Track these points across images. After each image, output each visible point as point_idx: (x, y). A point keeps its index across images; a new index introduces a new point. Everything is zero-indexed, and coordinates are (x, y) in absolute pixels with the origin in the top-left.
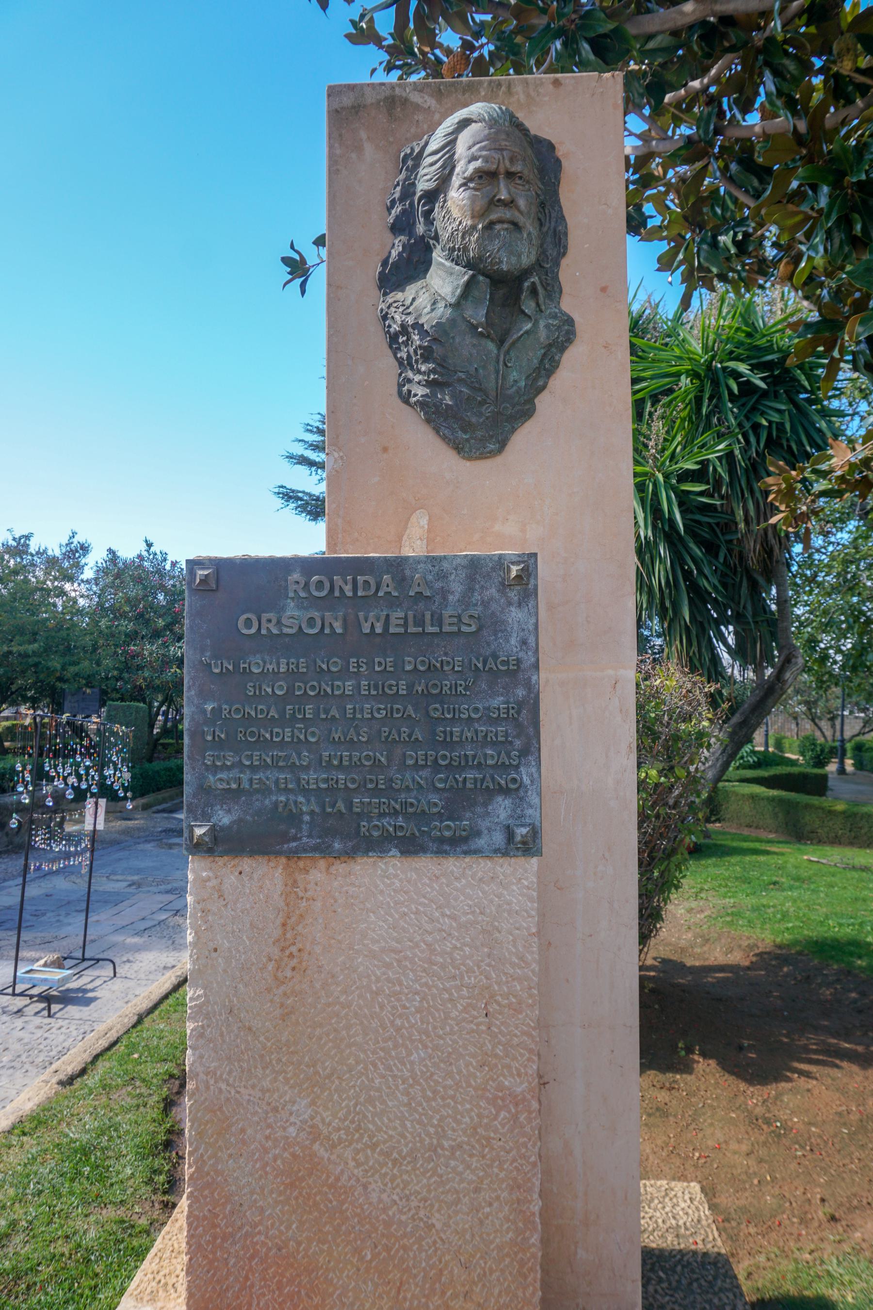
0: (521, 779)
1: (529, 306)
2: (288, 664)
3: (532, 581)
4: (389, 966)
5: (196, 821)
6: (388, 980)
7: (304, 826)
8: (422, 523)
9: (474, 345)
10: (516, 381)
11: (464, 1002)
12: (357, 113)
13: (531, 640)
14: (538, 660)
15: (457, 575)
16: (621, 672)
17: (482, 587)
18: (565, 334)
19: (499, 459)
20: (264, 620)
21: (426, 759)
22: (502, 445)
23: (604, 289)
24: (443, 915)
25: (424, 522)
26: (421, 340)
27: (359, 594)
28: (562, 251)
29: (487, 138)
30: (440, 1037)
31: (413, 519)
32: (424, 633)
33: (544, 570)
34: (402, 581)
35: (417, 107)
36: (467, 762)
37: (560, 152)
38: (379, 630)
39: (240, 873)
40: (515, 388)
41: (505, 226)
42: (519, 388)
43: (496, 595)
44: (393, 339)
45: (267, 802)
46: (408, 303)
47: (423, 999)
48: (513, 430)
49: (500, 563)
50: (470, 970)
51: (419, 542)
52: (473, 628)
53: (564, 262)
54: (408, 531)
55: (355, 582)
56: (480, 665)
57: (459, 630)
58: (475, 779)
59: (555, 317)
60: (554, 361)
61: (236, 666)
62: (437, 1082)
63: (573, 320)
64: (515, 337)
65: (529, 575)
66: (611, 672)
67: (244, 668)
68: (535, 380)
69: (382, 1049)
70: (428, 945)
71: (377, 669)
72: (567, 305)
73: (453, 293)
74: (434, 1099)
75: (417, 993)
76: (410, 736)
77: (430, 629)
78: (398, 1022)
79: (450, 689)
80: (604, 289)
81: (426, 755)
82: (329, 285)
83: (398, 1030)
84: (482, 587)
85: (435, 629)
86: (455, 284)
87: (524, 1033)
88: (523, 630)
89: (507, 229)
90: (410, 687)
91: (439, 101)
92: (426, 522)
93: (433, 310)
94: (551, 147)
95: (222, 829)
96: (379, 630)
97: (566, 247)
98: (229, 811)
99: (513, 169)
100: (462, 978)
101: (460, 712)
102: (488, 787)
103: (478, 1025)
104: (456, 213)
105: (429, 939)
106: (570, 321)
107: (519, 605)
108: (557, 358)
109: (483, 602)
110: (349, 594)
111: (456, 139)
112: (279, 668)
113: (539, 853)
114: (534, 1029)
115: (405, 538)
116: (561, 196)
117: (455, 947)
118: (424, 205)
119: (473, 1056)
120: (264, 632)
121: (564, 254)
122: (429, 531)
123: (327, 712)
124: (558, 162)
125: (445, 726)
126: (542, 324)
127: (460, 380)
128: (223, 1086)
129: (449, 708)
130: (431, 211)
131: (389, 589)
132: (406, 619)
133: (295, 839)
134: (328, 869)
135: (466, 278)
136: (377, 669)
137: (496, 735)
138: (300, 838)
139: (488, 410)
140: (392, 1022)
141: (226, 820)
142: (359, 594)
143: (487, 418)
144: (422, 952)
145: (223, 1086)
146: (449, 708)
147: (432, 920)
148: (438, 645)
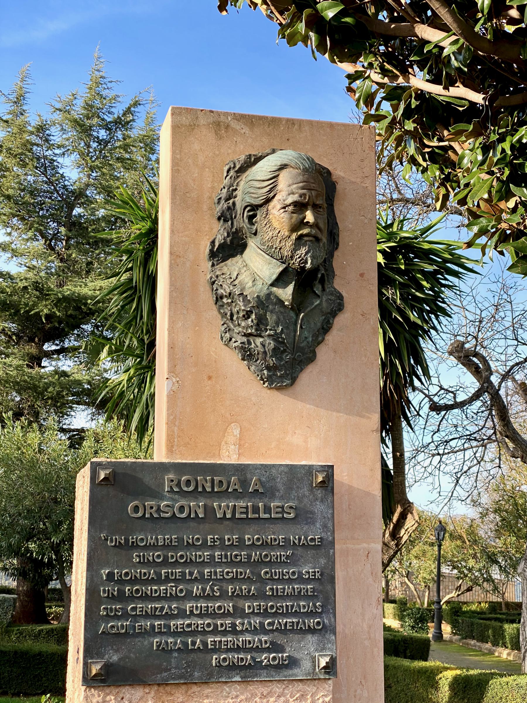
0: (324, 622)
1: (318, 289)
2: (164, 539)
3: (331, 485)
5: (92, 658)
7: (173, 660)
8: (235, 433)
9: (281, 312)
10: (306, 338)
12: (193, 129)
13: (330, 525)
14: (334, 538)
15: (281, 478)
16: (373, 545)
17: (298, 487)
18: (338, 305)
20: (148, 508)
21: (260, 609)
23: (362, 275)
25: (237, 432)
26: (245, 306)
27: (216, 490)
29: (301, 178)
32: (259, 518)
33: (338, 476)
34: (244, 483)
35: (235, 131)
36: (287, 610)
38: (229, 516)
39: (122, 698)
40: (305, 343)
41: (311, 238)
42: (308, 342)
43: (307, 493)
44: (219, 298)
45: (146, 643)
46: (234, 277)
48: (302, 370)
49: (309, 470)
51: (233, 447)
52: (292, 515)
54: (225, 438)
55: (213, 481)
56: (296, 542)
57: (283, 516)
58: (293, 622)
59: (332, 294)
60: (330, 324)
63: (343, 297)
64: (309, 309)
65: (329, 480)
66: (365, 545)
67: (133, 542)
68: (317, 337)
71: (227, 543)
72: (338, 284)
73: (270, 278)
79: (277, 558)
80: (362, 275)
81: (260, 605)
82: (171, 253)
84: (298, 487)
85: (267, 516)
86: (272, 271)
88: (325, 518)
89: (311, 241)
91: (251, 129)
92: (238, 432)
93: (253, 286)
95: (112, 665)
96: (229, 516)
97: (338, 244)
98: (117, 651)
99: (318, 203)
101: (283, 575)
102: (301, 628)
104: (276, 224)
106: (341, 297)
107: (322, 501)
108: (331, 321)
109: (298, 497)
110: (209, 489)
111: (278, 175)
112: (158, 543)
113: (335, 674)
115: (223, 443)
116: (335, 209)
118: (249, 211)
120: (147, 516)
121: (337, 248)
122: (240, 439)
125: (273, 585)
126: (324, 299)
129: (275, 572)
130: (255, 216)
131: (236, 487)
133: (166, 670)
134: (186, 692)
135: (281, 269)
136: (227, 543)
137: (307, 591)
138: (170, 670)
141: (115, 658)
142: (216, 490)
143: (286, 362)
146: (275, 572)
148: (269, 528)
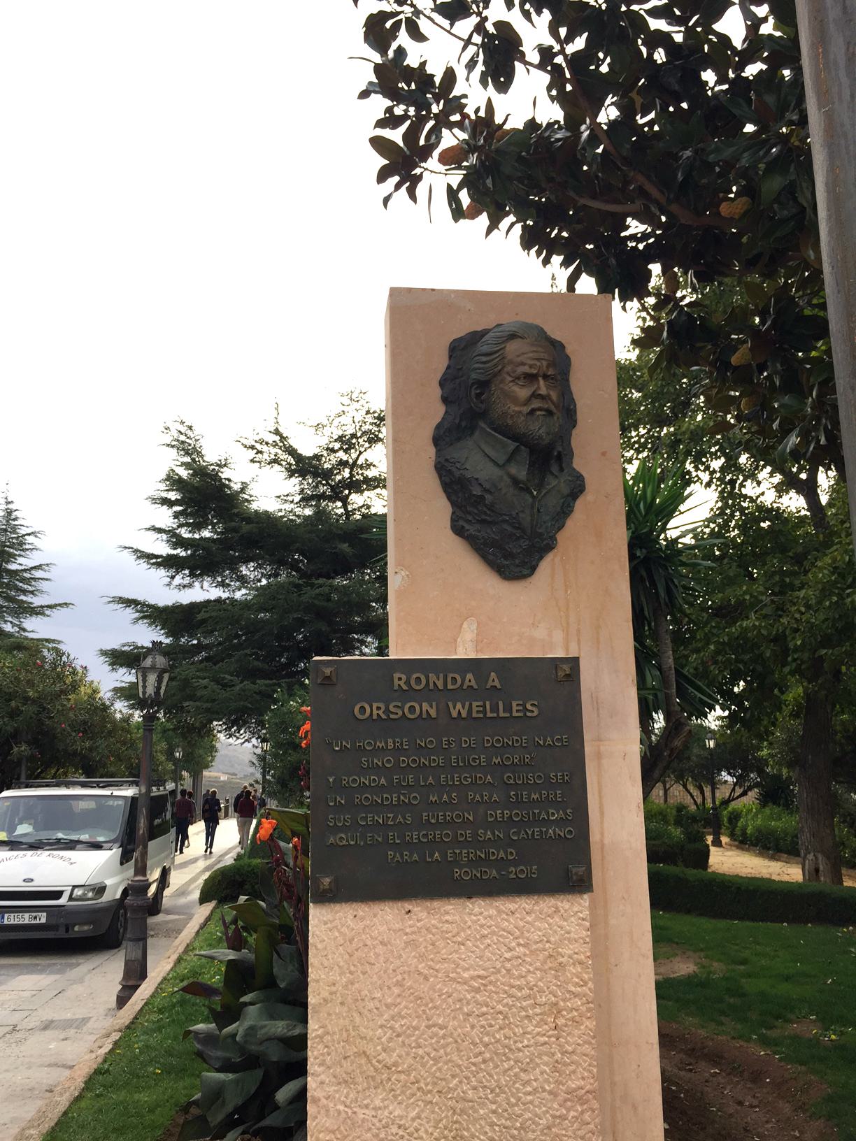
1: (555, 469)
4: (477, 990)
6: (477, 1003)
11: (538, 1018)
18: (577, 487)
19: (530, 580)
22: (533, 569)
23: (604, 454)
24: (519, 945)
28: (574, 423)
30: (519, 1050)
31: (465, 625)
37: (568, 351)
47: (506, 1017)
48: (541, 558)
50: (541, 991)
53: (574, 432)
61: (353, 744)
62: (518, 1089)
69: (474, 1064)
70: (508, 971)
72: (577, 464)
74: (517, 1105)
75: (500, 1013)
76: (490, 798)
77: (502, 714)
78: (486, 1039)
80: (604, 454)
83: (486, 1045)
87: (585, 1042)
90: (489, 760)
94: (563, 347)
100: (535, 998)
103: (549, 1037)
105: (508, 965)
114: (594, 1037)
117: (529, 971)
119: (546, 1064)
123: (425, 780)
124: (568, 358)
127: (505, 521)
128: (341, 1108)
132: (484, 706)
139: (524, 544)
140: (481, 1040)
144: (503, 976)
145: (341, 1108)
147: (510, 949)
